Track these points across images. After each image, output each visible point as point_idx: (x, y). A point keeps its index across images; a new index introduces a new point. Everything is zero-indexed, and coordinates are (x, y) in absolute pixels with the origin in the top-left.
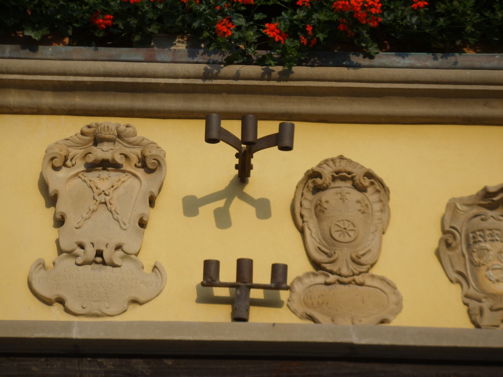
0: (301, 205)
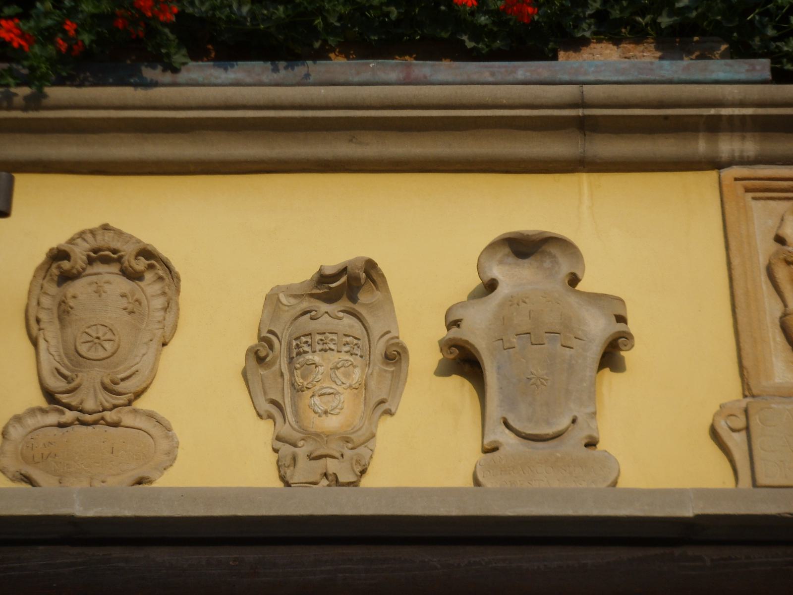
0: (38, 304)
